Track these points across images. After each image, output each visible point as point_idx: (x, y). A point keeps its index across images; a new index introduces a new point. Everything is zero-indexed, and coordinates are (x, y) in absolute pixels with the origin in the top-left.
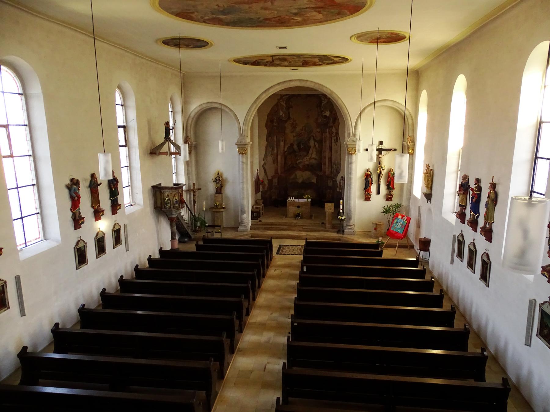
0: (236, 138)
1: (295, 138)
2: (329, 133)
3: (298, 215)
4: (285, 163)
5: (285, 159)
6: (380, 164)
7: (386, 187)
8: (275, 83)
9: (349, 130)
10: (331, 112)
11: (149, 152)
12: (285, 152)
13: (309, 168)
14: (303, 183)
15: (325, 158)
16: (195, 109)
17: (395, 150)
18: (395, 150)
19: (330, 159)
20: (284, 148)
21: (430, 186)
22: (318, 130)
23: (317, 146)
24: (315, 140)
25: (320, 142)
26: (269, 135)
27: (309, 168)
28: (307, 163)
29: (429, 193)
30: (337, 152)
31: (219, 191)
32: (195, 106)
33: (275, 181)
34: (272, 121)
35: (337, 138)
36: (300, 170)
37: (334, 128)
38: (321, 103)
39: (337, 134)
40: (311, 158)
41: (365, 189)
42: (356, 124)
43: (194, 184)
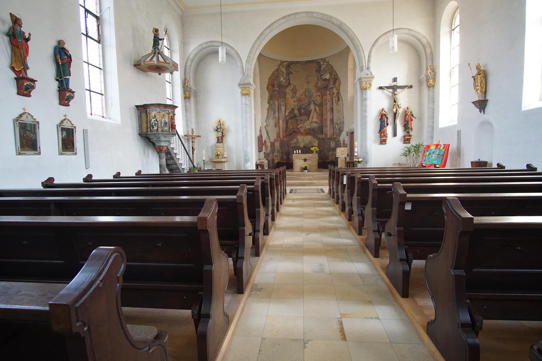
0: (239, 77)
1: (296, 103)
2: (330, 95)
3: (305, 168)
4: (287, 128)
5: (287, 123)
6: (395, 102)
7: (403, 128)
8: (281, 17)
9: (362, 63)
10: (331, 74)
11: (133, 63)
12: (286, 117)
13: (309, 132)
14: (304, 147)
15: (326, 120)
16: (194, 49)
17: (411, 87)
18: (411, 87)
19: (332, 120)
20: (285, 112)
21: (484, 90)
22: (318, 94)
23: (317, 110)
24: (315, 104)
25: (321, 105)
26: (271, 98)
27: (309, 132)
28: (308, 127)
29: (482, 98)
30: (339, 112)
31: (220, 140)
32: (193, 47)
33: (277, 144)
34: (273, 86)
35: (339, 98)
36: (302, 134)
37: (334, 89)
38: (320, 67)
39: (338, 93)
40: (311, 123)
41: (380, 131)
42: (369, 56)
43: (193, 129)
